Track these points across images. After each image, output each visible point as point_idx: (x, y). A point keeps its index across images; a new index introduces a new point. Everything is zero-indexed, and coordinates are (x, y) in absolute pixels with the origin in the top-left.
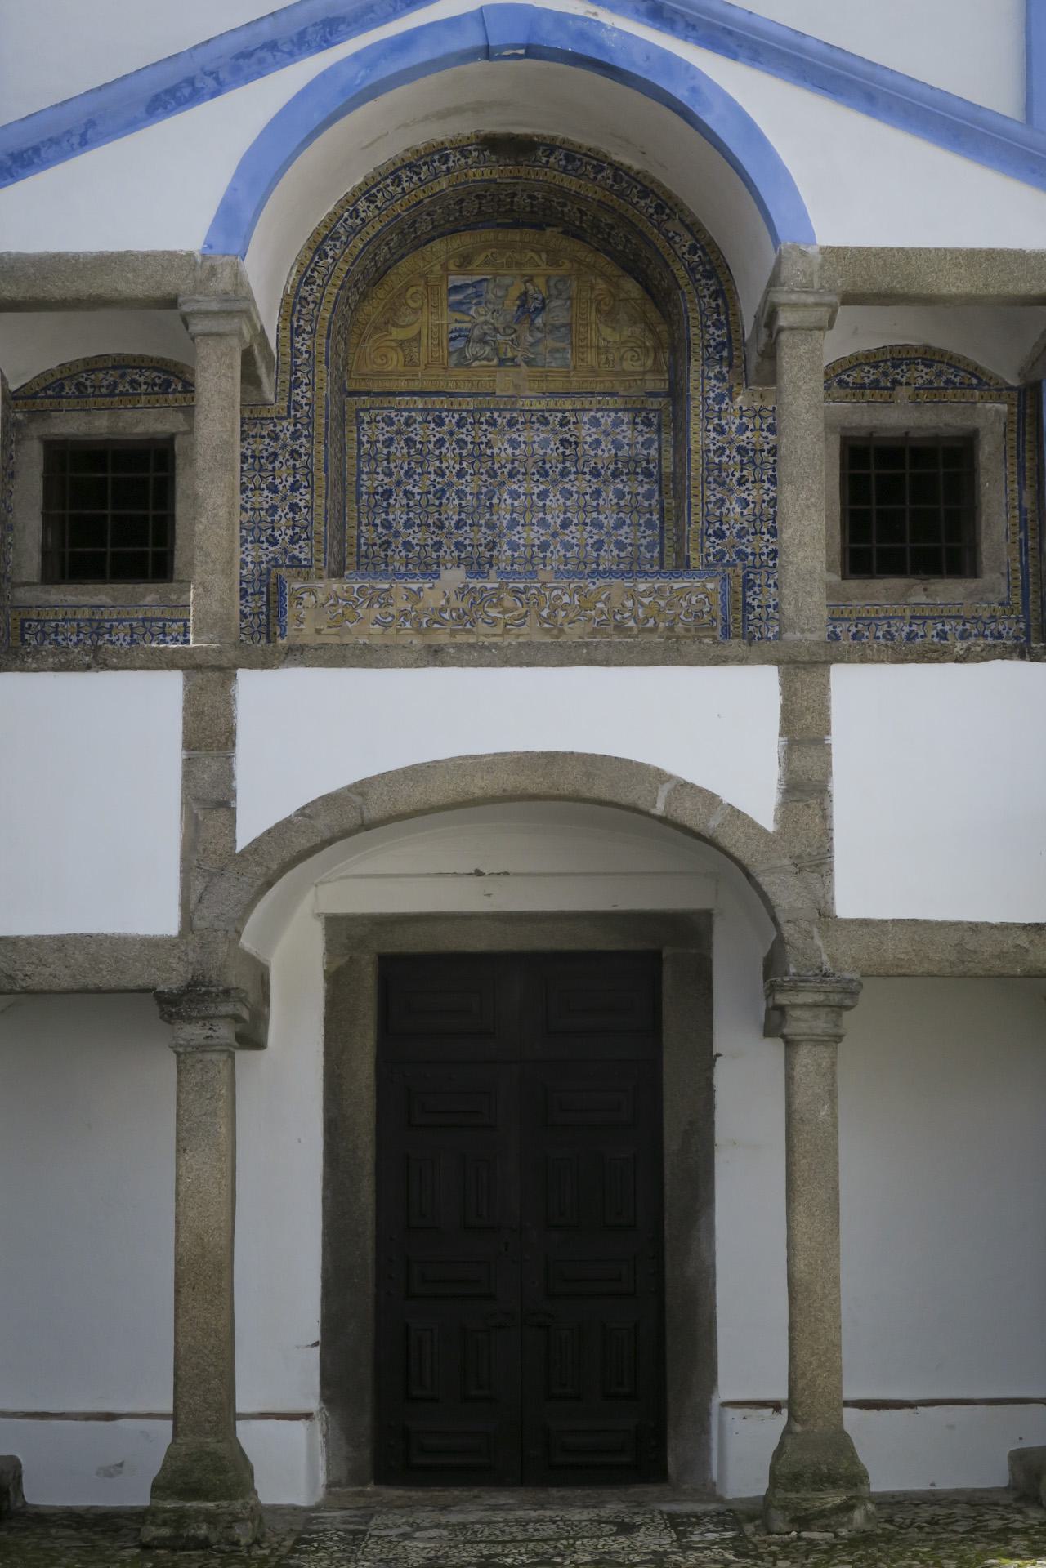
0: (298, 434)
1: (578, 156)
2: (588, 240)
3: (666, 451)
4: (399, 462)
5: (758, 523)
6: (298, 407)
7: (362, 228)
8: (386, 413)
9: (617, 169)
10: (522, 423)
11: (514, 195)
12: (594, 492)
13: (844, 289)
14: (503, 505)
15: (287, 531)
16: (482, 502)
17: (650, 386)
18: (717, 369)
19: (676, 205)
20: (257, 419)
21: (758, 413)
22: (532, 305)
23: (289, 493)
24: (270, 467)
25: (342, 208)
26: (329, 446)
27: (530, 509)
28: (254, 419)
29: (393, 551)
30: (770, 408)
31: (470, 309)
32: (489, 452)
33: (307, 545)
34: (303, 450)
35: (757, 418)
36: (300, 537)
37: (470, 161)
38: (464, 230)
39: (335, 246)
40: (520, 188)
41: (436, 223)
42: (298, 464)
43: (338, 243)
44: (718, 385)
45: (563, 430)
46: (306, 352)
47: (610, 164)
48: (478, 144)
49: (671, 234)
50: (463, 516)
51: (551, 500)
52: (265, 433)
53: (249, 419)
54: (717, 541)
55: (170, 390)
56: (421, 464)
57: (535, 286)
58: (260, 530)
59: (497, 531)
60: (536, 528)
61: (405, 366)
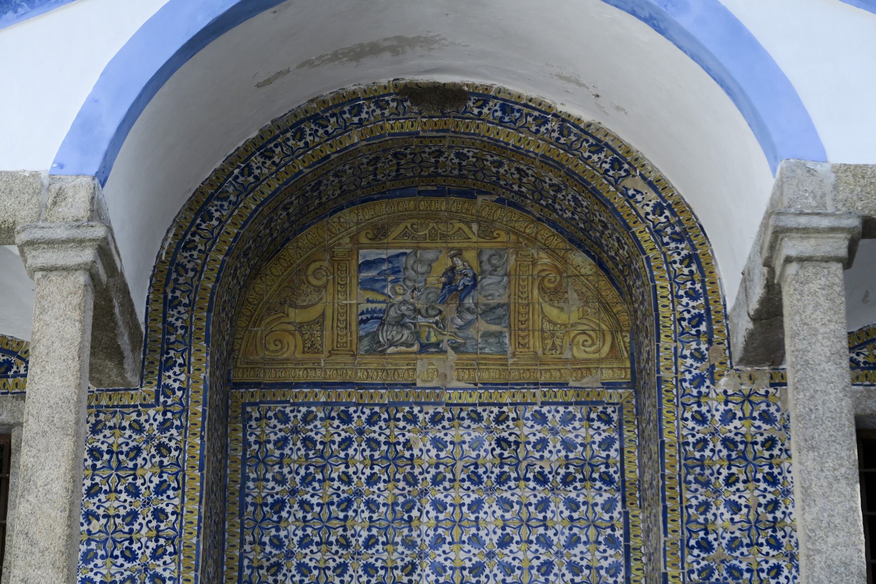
0: (168, 424)
1: (517, 107)
2: (529, 209)
3: (629, 452)
4: (295, 466)
5: (754, 531)
6: (169, 392)
7: (256, 186)
8: (279, 407)
9: (564, 120)
10: (449, 420)
11: (440, 153)
12: (540, 503)
13: (866, 212)
14: (424, 519)
15: (149, 544)
16: (399, 516)
17: (608, 375)
18: (694, 345)
19: (636, 160)
20: (117, 406)
21: (747, 398)
22: (461, 282)
23: (153, 496)
24: (131, 465)
25: (232, 164)
26: (205, 439)
27: (459, 523)
28: (113, 407)
29: (285, 575)
30: (762, 392)
31: (385, 287)
32: (407, 454)
33: (173, 561)
34: (173, 444)
35: (746, 404)
36: (166, 550)
37: (387, 112)
38: (378, 199)
39: (222, 206)
40: (446, 143)
41: (345, 187)
42: (166, 461)
43: (226, 204)
44: (695, 364)
45: (501, 427)
46: (182, 328)
47: (555, 115)
48: (397, 94)
49: (631, 192)
50: (374, 531)
51: (486, 513)
52: (126, 424)
53: (107, 406)
54: (702, 555)
55: (11, 373)
56: (322, 468)
57: (463, 260)
58: (114, 541)
59: (417, 550)
60: (467, 547)
61: (303, 352)
